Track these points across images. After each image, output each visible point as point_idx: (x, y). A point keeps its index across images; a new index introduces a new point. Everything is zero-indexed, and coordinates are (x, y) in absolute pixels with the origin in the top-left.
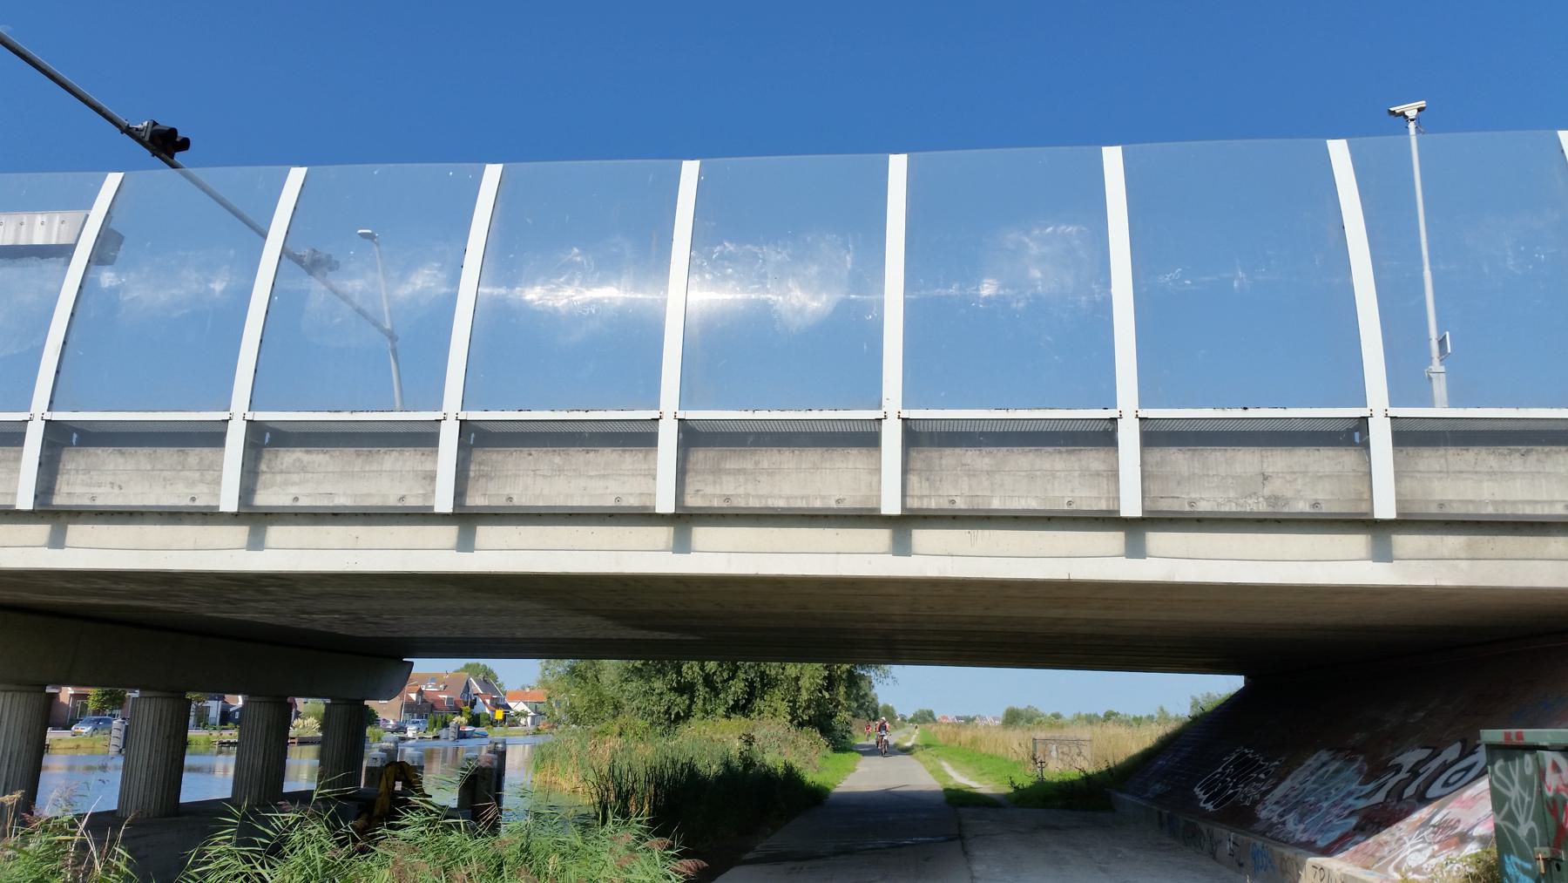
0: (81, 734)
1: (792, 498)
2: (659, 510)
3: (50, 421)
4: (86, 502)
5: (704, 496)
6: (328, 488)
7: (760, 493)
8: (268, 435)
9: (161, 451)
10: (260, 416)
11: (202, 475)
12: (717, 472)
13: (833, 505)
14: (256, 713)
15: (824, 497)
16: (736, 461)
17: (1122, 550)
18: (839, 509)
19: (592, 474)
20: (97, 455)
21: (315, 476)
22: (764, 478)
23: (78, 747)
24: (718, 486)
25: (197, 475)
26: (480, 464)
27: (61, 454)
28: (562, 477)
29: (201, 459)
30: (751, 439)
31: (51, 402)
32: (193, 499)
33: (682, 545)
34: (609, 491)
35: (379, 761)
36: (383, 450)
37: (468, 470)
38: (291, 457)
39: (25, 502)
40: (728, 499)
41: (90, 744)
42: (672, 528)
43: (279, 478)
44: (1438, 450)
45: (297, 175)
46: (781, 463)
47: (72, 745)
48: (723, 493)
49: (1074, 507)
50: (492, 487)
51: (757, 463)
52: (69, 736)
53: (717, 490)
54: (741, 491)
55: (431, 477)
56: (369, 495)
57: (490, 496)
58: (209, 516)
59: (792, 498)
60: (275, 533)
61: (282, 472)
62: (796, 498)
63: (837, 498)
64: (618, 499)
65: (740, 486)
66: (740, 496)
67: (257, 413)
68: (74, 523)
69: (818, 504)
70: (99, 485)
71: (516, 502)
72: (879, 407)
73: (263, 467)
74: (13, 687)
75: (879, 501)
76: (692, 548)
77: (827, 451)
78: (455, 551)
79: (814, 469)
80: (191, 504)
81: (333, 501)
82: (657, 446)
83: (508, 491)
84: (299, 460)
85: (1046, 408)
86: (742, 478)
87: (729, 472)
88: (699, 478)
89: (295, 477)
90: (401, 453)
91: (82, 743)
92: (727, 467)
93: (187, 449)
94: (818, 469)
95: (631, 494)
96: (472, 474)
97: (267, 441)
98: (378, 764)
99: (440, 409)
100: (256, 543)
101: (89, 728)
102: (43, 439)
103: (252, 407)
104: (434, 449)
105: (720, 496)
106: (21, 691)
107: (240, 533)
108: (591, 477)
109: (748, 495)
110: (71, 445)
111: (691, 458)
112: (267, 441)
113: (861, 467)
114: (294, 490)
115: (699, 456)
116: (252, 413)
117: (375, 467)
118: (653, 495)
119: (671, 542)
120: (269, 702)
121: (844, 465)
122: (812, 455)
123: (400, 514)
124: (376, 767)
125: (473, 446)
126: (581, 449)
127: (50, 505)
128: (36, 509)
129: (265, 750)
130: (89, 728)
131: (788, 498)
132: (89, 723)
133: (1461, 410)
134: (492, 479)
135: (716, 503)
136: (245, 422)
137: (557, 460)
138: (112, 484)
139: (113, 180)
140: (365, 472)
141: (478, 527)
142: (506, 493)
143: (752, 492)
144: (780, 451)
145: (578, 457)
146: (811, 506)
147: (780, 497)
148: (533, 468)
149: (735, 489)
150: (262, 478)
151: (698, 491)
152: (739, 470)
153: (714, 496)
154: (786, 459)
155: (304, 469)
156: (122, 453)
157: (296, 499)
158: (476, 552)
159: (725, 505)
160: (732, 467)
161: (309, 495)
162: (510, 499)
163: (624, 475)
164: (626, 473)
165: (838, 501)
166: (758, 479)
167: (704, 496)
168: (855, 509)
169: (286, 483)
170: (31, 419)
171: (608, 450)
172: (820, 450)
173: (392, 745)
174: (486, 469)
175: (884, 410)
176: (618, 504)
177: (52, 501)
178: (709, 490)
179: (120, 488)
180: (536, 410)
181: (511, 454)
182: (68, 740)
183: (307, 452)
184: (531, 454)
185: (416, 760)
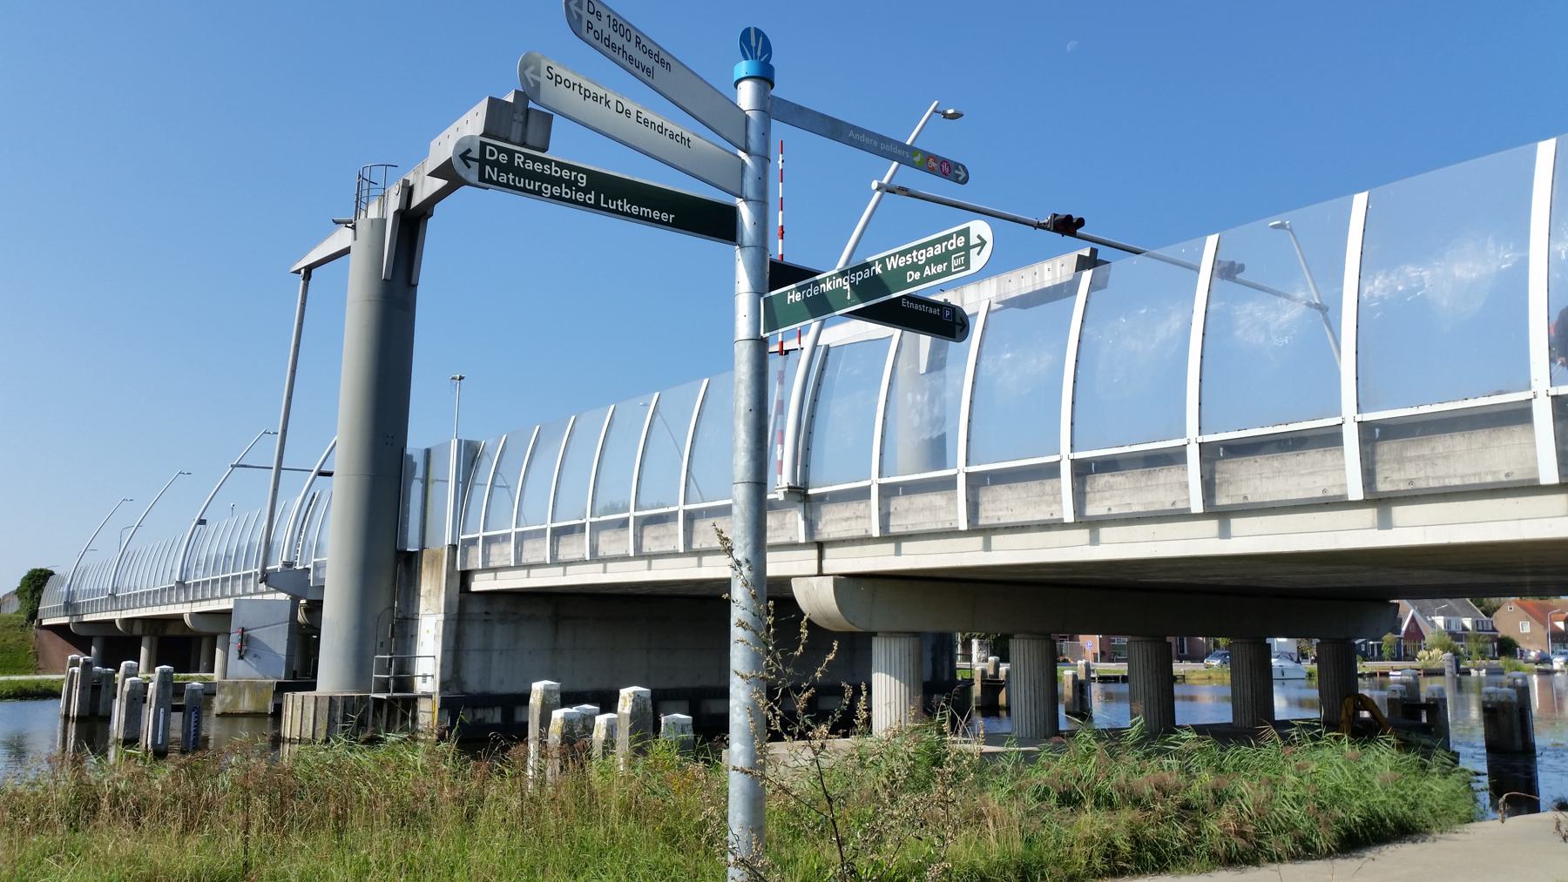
0: (1211, 666)
1: (1466, 476)
2: (1351, 498)
3: (1362, 422)
4: (995, 521)
5: (1392, 481)
6: (1127, 500)
7: (1440, 474)
8: (1377, 431)
9: (1031, 484)
10: (1368, 417)
11: (1055, 497)
12: (1401, 461)
13: (1503, 478)
14: (1240, 652)
15: (1494, 473)
16: (1415, 449)
17: (1088, 541)
18: (1509, 482)
19: (1302, 472)
20: (997, 491)
21: (1118, 492)
22: (1440, 462)
23: (1210, 678)
24: (1402, 473)
25: (1052, 497)
26: (1222, 473)
27: (978, 493)
28: (1281, 477)
29: (1053, 488)
30: (533, 534)
31: (967, 460)
32: (1052, 514)
33: (1385, 523)
34: (1317, 485)
35: (1398, 692)
36: (1157, 469)
37: (1214, 479)
38: (1103, 480)
39: (802, 539)
40: (1411, 482)
41: (1219, 676)
42: (1375, 510)
43: (1098, 495)
44: (1298, 455)
45: (1360, 201)
46: (1453, 446)
47: (1203, 676)
48: (1406, 478)
49: (1510, 479)
50: (1232, 490)
51: (1433, 449)
52: (1203, 669)
53: (1402, 475)
54: (1422, 474)
55: (1186, 486)
56: (1153, 503)
57: (1232, 496)
58: (953, 533)
59: (1466, 476)
60: (1399, 512)
61: (1099, 491)
62: (1469, 475)
63: (1506, 472)
64: (791, 538)
65: (1421, 470)
66: (1420, 478)
67: (1204, 436)
68: (994, 535)
69: (1489, 479)
70: (1001, 510)
71: (1251, 499)
72: (1529, 388)
73: (1088, 489)
74: (1029, 636)
75: (1535, 469)
76: (1232, 534)
77: (1494, 431)
78: (1376, 530)
79: (1482, 448)
80: (1051, 518)
81: (1397, 486)
82: (1186, 463)
83: (1244, 492)
84: (1108, 482)
85: (1449, 401)
86: (1421, 464)
87: (1411, 460)
88: (1387, 467)
89: (1107, 494)
90: (1169, 470)
91: (1212, 674)
92: (1409, 455)
93: (1045, 481)
94: (1486, 448)
95: (1334, 486)
96: (1217, 481)
97: (1377, 436)
98: (1398, 696)
99: (1341, 415)
100: (1094, 541)
101: (1219, 661)
102: (966, 484)
103: (1553, 381)
104: (1527, 427)
105: (1406, 480)
106: (1033, 639)
107: (1369, 514)
108: (1303, 475)
109: (1428, 478)
110: (898, 495)
111: (1378, 450)
112: (1377, 436)
113: (1526, 442)
114: (1108, 503)
115: (1386, 450)
116: (1360, 415)
117: (1154, 482)
118: (1344, 485)
119: (1376, 521)
120: (1241, 643)
121: (1510, 442)
122: (1481, 436)
123: (1291, 507)
124: (1396, 699)
125: (1378, 440)
126: (1292, 453)
127: (977, 525)
128: (1564, 481)
129: (1252, 683)
130: (1219, 661)
131: (1462, 477)
132: (1217, 657)
133: (1389, 411)
134: (1231, 483)
135: (1403, 486)
136: (1550, 398)
137: (1276, 464)
138: (1007, 508)
139: (1360, 201)
140: (1148, 486)
141: (1232, 520)
142: (1243, 493)
143: (1431, 475)
144: (1451, 436)
145: (1292, 460)
146: (1483, 481)
147: (1455, 476)
148: (1259, 472)
149: (1417, 472)
150: (1089, 497)
151: (1387, 478)
152: (1418, 457)
153: (1400, 480)
154: (1457, 443)
155: (1111, 488)
156: (1010, 488)
157: (1110, 509)
158: (1394, 529)
159: (1410, 487)
160: (1413, 454)
161: (1116, 506)
162: (1246, 497)
163: (1327, 471)
164: (1328, 468)
165: (1507, 475)
166: (506, 553)
167: (1392, 481)
168: (1524, 481)
169: (1102, 499)
170: (1189, 443)
171: (1313, 451)
172: (1487, 431)
173: (1411, 678)
174: (1226, 476)
175: (1533, 390)
176: (1325, 495)
177: (1085, 512)
178: (1395, 476)
179: (1012, 510)
180: (1250, 428)
181: (1243, 463)
182: (1200, 672)
183: (1112, 475)
184: (1256, 462)
185: (1436, 693)
